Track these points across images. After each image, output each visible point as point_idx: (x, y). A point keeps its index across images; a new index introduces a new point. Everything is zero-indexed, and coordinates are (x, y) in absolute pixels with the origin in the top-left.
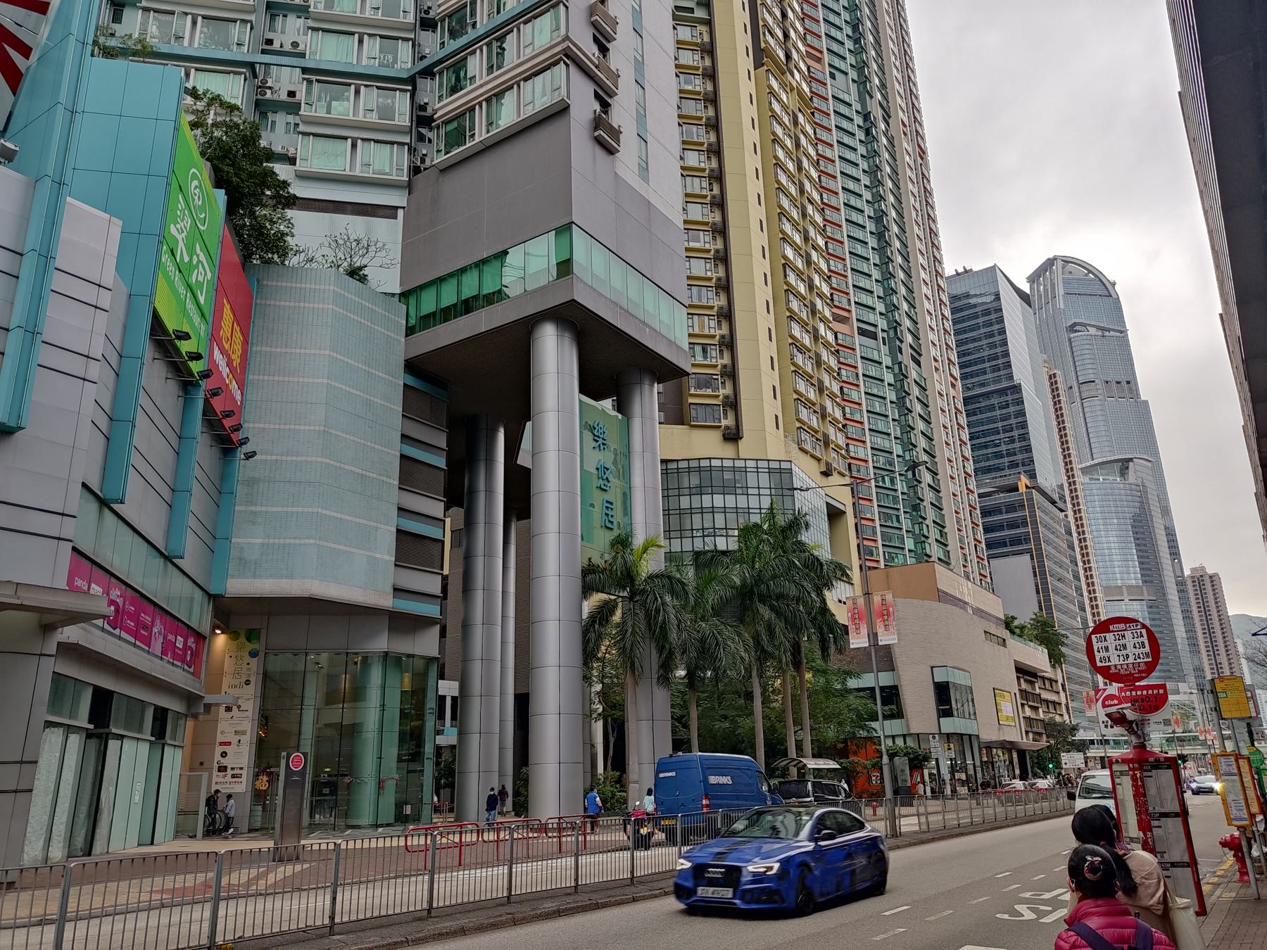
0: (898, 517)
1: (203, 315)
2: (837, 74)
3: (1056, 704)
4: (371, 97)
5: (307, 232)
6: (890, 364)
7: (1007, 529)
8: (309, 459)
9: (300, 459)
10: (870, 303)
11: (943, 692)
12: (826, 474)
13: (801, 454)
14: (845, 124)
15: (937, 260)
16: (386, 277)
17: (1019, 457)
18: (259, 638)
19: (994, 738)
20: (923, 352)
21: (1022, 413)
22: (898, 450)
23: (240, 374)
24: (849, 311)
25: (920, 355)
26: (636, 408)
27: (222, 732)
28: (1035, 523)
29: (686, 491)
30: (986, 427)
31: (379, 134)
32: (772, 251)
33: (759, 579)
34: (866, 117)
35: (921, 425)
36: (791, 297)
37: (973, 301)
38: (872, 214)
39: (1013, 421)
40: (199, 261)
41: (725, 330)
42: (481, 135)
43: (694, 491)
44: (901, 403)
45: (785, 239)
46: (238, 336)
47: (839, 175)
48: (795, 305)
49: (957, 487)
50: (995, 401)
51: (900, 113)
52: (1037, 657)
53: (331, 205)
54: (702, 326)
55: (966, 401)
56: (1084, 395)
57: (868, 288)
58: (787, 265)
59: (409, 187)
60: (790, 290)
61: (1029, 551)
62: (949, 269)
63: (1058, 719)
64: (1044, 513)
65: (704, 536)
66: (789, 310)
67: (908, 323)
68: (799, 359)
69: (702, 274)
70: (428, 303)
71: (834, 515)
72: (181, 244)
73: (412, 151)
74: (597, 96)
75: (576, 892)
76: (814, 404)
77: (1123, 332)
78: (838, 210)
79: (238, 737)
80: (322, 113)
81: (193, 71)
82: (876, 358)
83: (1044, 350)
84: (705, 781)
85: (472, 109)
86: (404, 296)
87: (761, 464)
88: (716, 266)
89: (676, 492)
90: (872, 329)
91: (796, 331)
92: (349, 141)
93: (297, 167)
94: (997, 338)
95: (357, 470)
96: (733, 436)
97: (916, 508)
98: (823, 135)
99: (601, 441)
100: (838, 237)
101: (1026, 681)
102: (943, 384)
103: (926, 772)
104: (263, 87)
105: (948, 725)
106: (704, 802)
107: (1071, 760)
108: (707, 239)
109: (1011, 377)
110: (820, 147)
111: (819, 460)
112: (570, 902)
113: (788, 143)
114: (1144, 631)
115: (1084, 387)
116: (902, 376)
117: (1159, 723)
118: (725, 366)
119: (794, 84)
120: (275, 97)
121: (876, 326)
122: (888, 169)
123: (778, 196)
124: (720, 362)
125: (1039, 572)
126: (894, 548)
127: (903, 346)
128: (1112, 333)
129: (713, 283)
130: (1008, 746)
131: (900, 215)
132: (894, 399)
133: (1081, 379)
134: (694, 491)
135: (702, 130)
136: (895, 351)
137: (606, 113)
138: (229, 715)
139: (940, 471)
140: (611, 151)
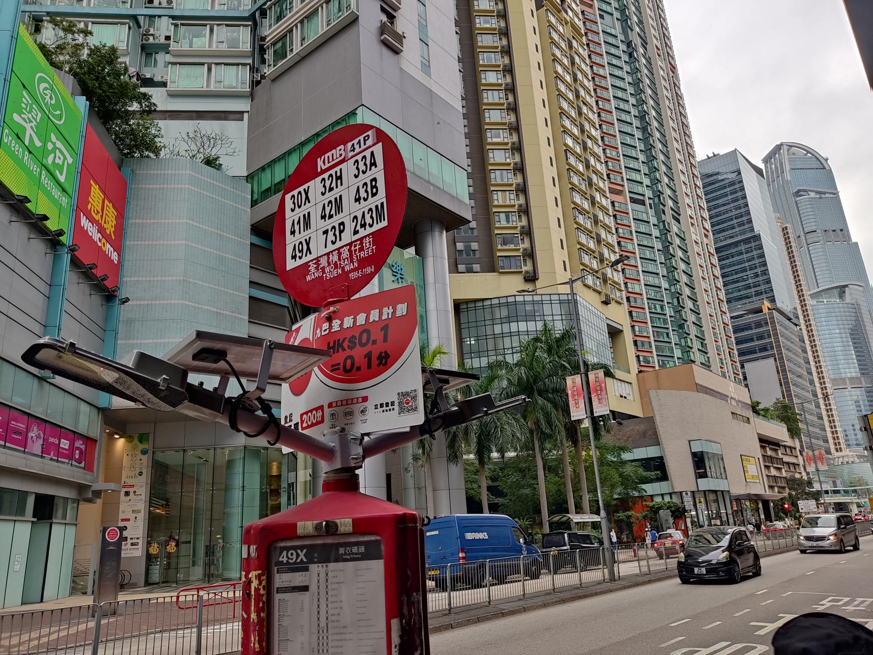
0: (667, 334)
1: (64, 190)
2: (605, 15)
3: (795, 465)
4: (222, 32)
5: (171, 134)
6: (656, 223)
7: (754, 340)
8: (173, 302)
9: (165, 302)
10: (639, 179)
11: (699, 461)
12: (606, 303)
13: (585, 290)
14: (613, 51)
15: (689, 145)
16: (236, 164)
17: (763, 287)
18: (148, 440)
19: (743, 492)
20: (682, 212)
21: (762, 256)
22: (665, 284)
23: (118, 240)
24: (623, 186)
25: (679, 215)
26: (429, 251)
27: (123, 512)
28: (776, 334)
29: (498, 321)
30: (736, 267)
31: (228, 59)
32: (555, 140)
33: (536, 378)
34: (629, 44)
35: (682, 266)
36: (572, 174)
37: (720, 178)
38: (637, 114)
39: (756, 261)
40: (55, 148)
41: (522, 201)
42: (297, 47)
43: (504, 320)
44: (666, 250)
45: (566, 131)
46: (111, 212)
47: (610, 87)
48: (575, 180)
49: (713, 313)
50: (743, 247)
51: (655, 40)
52: (778, 431)
53: (195, 114)
54: (504, 199)
55: (718, 250)
56: (809, 242)
57: (636, 168)
58: (568, 150)
59: (252, 96)
60: (571, 169)
61: (773, 355)
62: (701, 153)
63: (797, 476)
64: (781, 325)
65: (513, 353)
66: (571, 183)
67: (669, 192)
68: (581, 219)
69: (503, 161)
70: (266, 181)
71: (614, 333)
72: (29, 131)
73: (253, 69)
74: (383, 9)
75: (450, 613)
76: (594, 252)
77: (836, 194)
78: (611, 112)
79: (135, 515)
80: (185, 47)
81: (90, 24)
82: (645, 218)
83: (776, 209)
84: (462, 537)
85: (291, 31)
86: (250, 178)
87: (553, 297)
88: (513, 154)
89: (474, 324)
90: (641, 198)
91: (578, 199)
92: (206, 65)
93: (171, 87)
94: (741, 202)
95: (213, 309)
96: (531, 278)
97: (681, 326)
98: (597, 59)
99: (399, 276)
100: (612, 132)
101: (771, 449)
102: (698, 236)
103: (688, 520)
104: (146, 35)
105: (704, 484)
106: (461, 555)
107: (806, 506)
108: (505, 135)
109: (752, 230)
110: (595, 68)
111: (600, 293)
112: (646, 579)
113: (565, 61)
114: (378, 150)
115: (808, 236)
116: (665, 231)
117: (386, 406)
118: (523, 227)
119: (568, 19)
120: (157, 41)
121: (644, 195)
122: (648, 81)
123: (559, 101)
124: (519, 224)
125: (782, 370)
126: (665, 356)
127: (666, 209)
128: (827, 195)
129: (511, 167)
130: (755, 499)
131: (659, 114)
132: (661, 248)
133: (806, 230)
134: (504, 320)
135: (499, 56)
136: (660, 213)
137: (392, 23)
138: (128, 498)
139: (699, 299)
140: (396, 52)
